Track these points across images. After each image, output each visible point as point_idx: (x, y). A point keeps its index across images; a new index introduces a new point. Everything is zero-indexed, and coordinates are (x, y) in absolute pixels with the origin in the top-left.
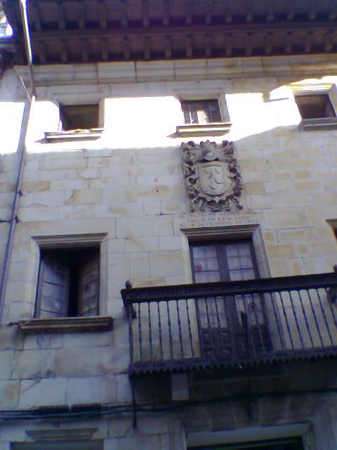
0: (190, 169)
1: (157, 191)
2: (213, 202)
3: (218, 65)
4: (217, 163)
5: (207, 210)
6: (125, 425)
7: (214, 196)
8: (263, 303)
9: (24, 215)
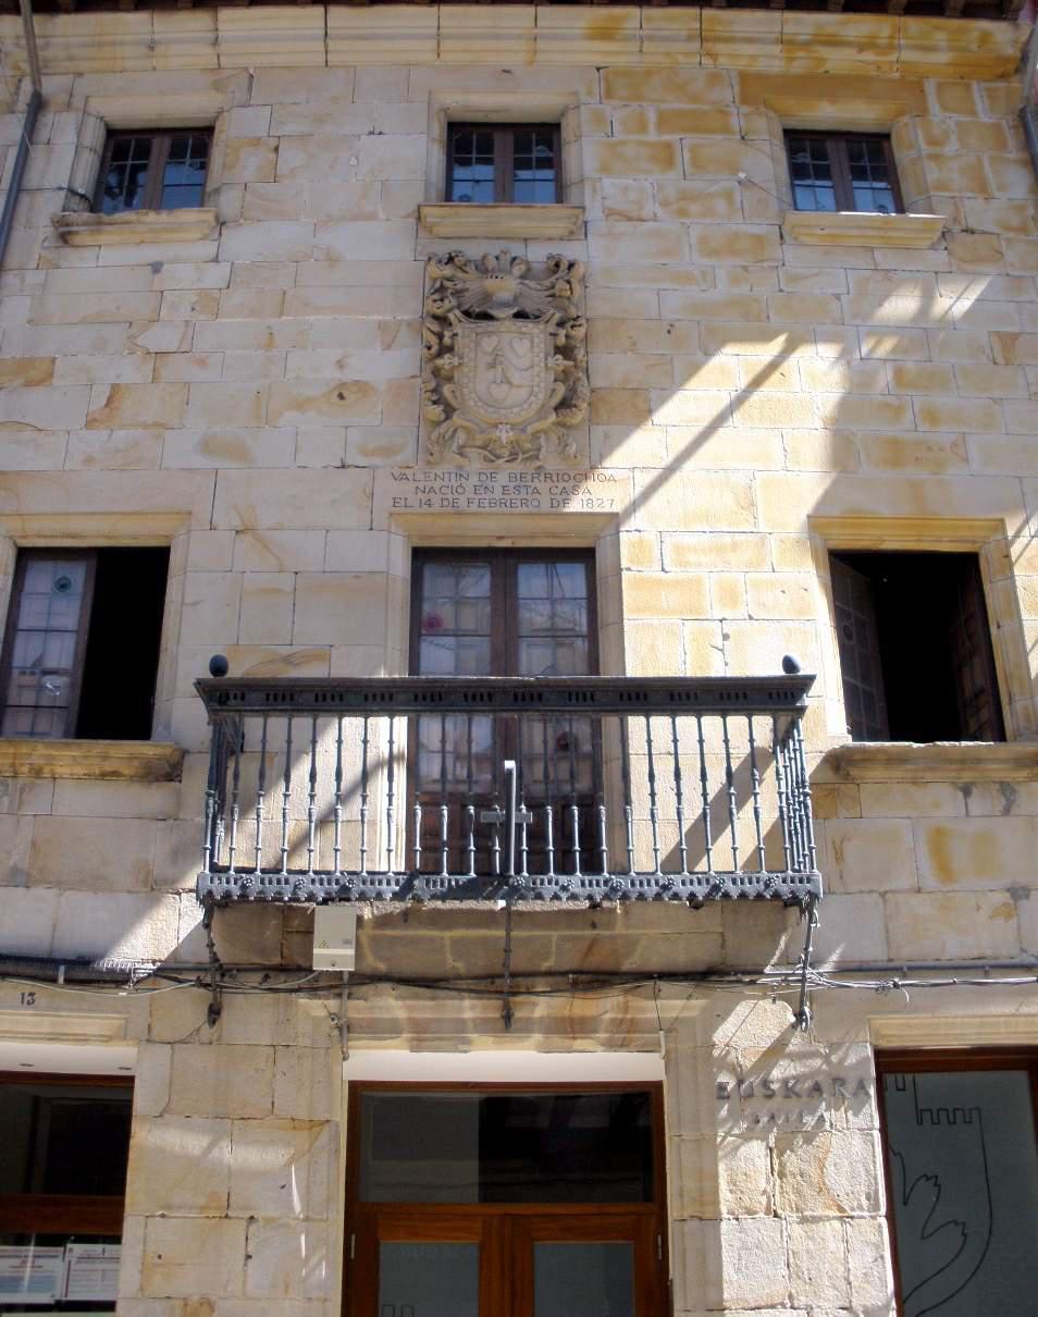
0: (440, 336)
1: (341, 397)
8: (596, 733)
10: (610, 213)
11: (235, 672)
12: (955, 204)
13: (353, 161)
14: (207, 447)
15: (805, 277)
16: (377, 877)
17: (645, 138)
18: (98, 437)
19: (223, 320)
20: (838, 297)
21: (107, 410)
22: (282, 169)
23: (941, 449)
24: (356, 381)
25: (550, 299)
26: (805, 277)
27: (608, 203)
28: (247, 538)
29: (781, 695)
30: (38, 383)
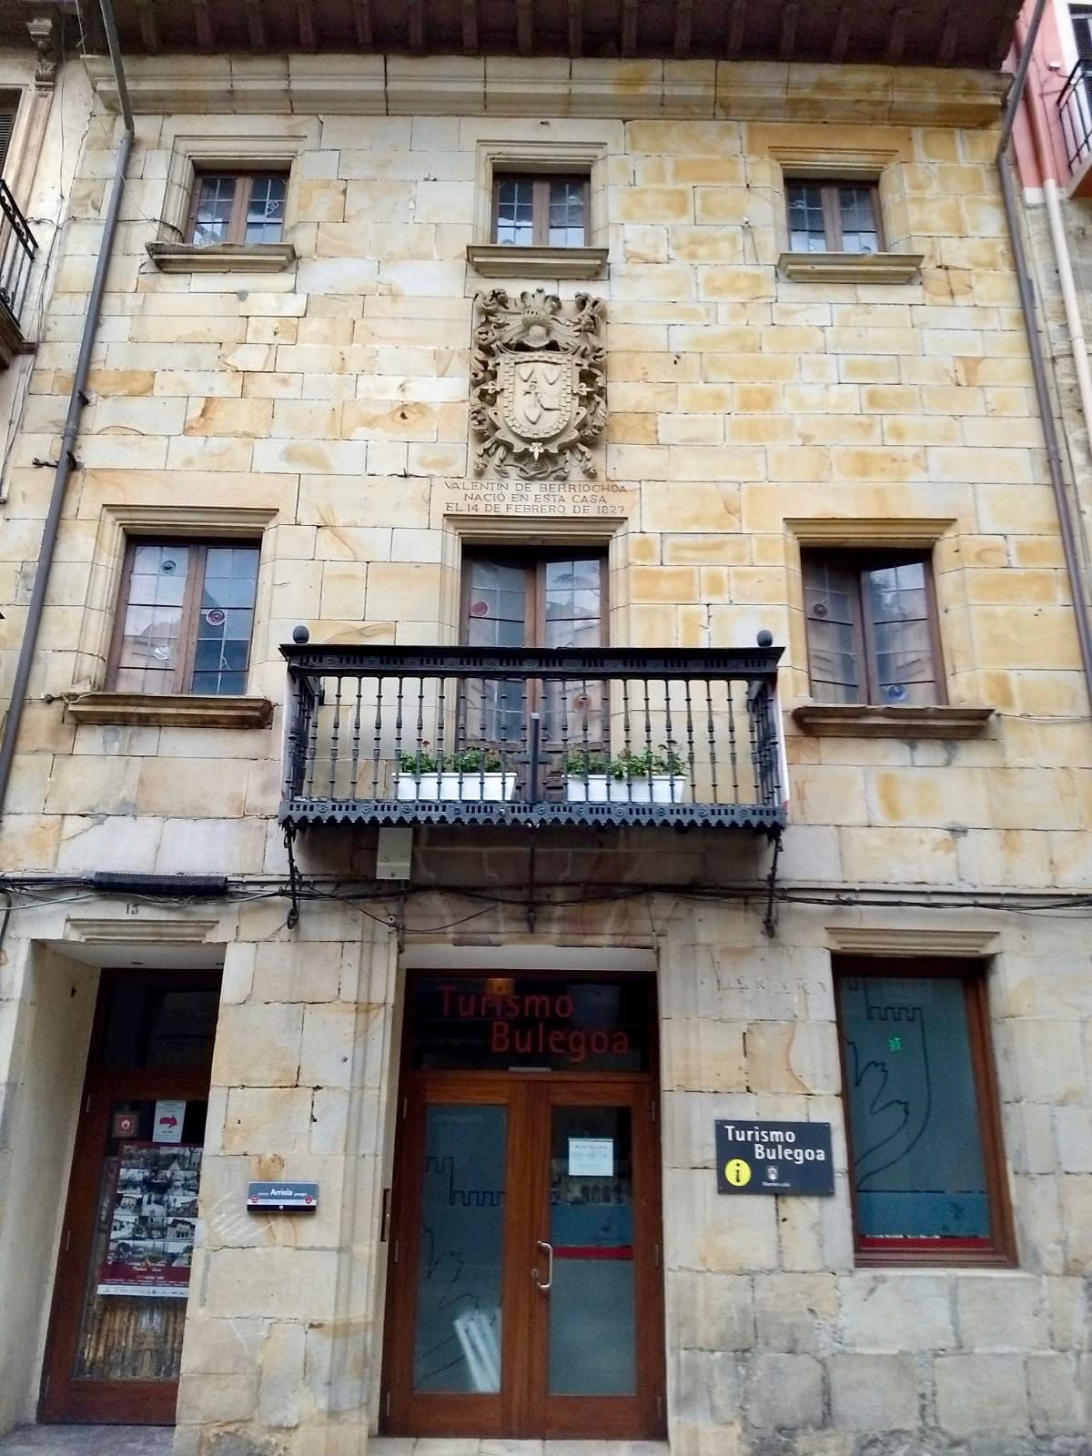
0: (485, 364)
1: (403, 416)
2: (525, 455)
3: (600, 77)
4: (554, 356)
5: (513, 472)
6: (274, 920)
7: (529, 441)
9: (92, 453)
10: (630, 257)
11: (315, 639)
12: (932, 243)
13: (411, 205)
14: (289, 455)
15: (794, 312)
16: (427, 805)
17: (661, 186)
18: (195, 442)
19: (302, 345)
20: (822, 328)
21: (202, 420)
22: (350, 211)
23: (905, 461)
24: (416, 403)
25: (578, 334)
26: (794, 312)
27: (629, 247)
28: (326, 533)
29: (755, 664)
30: (141, 394)
